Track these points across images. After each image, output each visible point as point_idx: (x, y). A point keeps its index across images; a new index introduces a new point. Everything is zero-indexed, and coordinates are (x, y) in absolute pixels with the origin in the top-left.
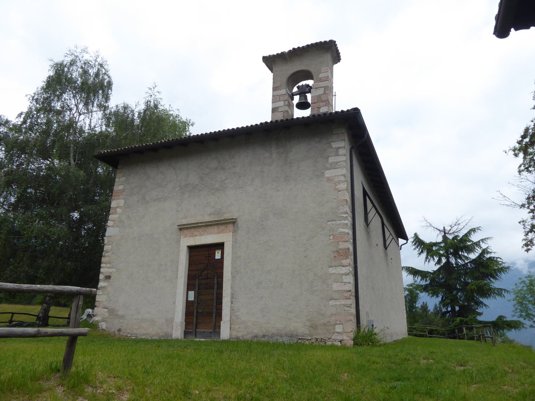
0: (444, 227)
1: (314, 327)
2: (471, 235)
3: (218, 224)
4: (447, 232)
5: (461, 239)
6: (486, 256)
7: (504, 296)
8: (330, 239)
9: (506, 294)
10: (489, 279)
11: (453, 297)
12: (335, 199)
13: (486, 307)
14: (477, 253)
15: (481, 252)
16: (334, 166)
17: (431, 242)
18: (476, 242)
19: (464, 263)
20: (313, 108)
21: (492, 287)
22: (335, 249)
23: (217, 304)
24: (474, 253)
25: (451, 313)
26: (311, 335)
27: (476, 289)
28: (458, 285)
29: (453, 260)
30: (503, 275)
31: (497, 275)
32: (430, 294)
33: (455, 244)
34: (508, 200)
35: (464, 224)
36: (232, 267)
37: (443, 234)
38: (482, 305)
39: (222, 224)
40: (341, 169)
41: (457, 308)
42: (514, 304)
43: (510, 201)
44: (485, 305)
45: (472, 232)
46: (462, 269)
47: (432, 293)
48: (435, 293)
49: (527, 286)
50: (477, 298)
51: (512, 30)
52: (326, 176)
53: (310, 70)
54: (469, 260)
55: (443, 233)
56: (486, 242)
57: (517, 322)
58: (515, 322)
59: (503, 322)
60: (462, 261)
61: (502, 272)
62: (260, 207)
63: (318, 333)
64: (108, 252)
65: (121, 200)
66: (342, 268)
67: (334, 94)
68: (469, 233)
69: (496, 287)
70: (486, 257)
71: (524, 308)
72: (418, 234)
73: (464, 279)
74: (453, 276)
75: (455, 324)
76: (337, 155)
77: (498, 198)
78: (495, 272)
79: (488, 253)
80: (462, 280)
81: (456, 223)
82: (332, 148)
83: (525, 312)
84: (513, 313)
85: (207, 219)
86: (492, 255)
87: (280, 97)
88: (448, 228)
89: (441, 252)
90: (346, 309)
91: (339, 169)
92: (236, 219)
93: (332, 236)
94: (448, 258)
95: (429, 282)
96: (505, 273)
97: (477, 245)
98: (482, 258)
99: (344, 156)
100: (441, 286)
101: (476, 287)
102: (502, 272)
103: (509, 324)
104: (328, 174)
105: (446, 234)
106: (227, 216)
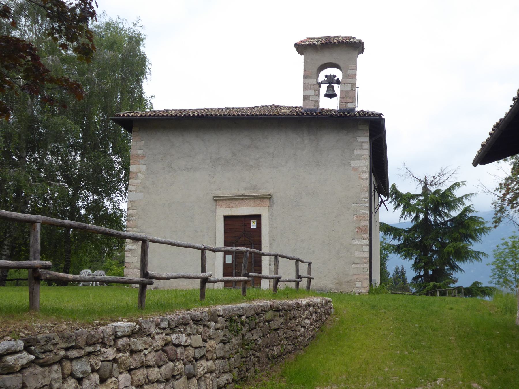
0: (426, 177)
1: (339, 283)
2: (454, 190)
3: (255, 198)
4: (429, 183)
5: (443, 193)
6: (467, 214)
7: (481, 260)
8: (354, 218)
9: (483, 258)
10: (468, 241)
11: (427, 260)
12: (359, 185)
13: (461, 271)
14: (459, 210)
15: (463, 209)
16: (359, 158)
17: (408, 193)
18: (459, 198)
19: (443, 221)
20: (342, 103)
21: (470, 250)
22: (357, 226)
23: (254, 266)
24: (455, 210)
25: (423, 277)
26: (337, 289)
27: (453, 252)
28: (434, 246)
29: (432, 218)
30: (483, 237)
31: (477, 235)
32: (403, 256)
33: (436, 199)
34: (484, 188)
35: (448, 175)
36: (269, 236)
37: (424, 185)
38: (458, 269)
39: (258, 199)
40: (364, 161)
41: (431, 272)
42: (492, 269)
43: (486, 189)
44: (461, 269)
45: (456, 187)
46: (440, 228)
47: (405, 255)
48: (408, 255)
49: (509, 249)
50: (453, 262)
51: (479, 164)
52: (352, 165)
53: (340, 65)
54: (449, 217)
55: (424, 184)
56: (469, 199)
57: (492, 288)
58: (490, 289)
59: (477, 288)
60: (441, 219)
61: (482, 233)
62: (294, 187)
63: (342, 288)
64: (133, 217)
65: (142, 165)
66: (362, 240)
67: (357, 87)
68: (453, 187)
69: (474, 250)
70: (468, 216)
71: (502, 273)
72: (302, 37)
73: (441, 240)
74: (430, 236)
75: (428, 289)
76: (362, 148)
77: (478, 186)
78: (475, 233)
79: (470, 211)
80: (439, 240)
81: (440, 174)
82: (358, 142)
83: (503, 278)
84: (490, 279)
85: (243, 192)
86: (474, 214)
87: (311, 86)
88: (430, 179)
89: (420, 207)
90: (364, 271)
91: (362, 161)
92: (272, 196)
93: (355, 216)
94: (426, 214)
95: (402, 242)
96: (486, 234)
97: (459, 201)
98: (464, 217)
99: (367, 150)
100: (416, 246)
101: (454, 249)
102: (482, 233)
103: (484, 291)
104: (354, 164)
105: (427, 186)
106: (262, 192)
